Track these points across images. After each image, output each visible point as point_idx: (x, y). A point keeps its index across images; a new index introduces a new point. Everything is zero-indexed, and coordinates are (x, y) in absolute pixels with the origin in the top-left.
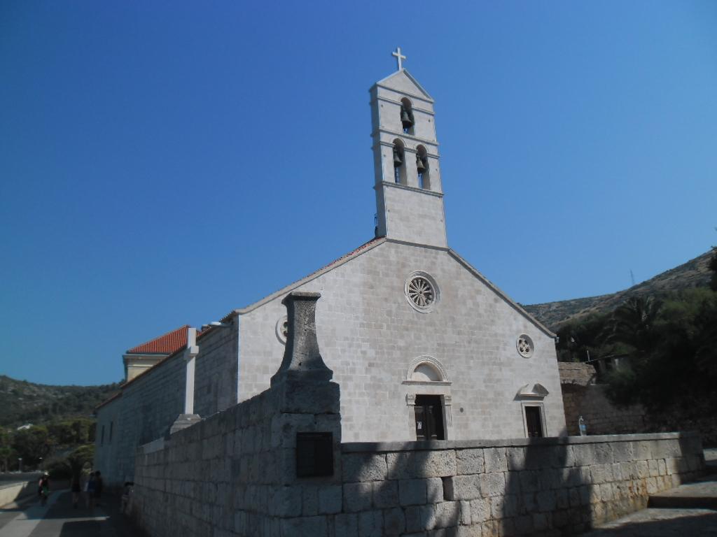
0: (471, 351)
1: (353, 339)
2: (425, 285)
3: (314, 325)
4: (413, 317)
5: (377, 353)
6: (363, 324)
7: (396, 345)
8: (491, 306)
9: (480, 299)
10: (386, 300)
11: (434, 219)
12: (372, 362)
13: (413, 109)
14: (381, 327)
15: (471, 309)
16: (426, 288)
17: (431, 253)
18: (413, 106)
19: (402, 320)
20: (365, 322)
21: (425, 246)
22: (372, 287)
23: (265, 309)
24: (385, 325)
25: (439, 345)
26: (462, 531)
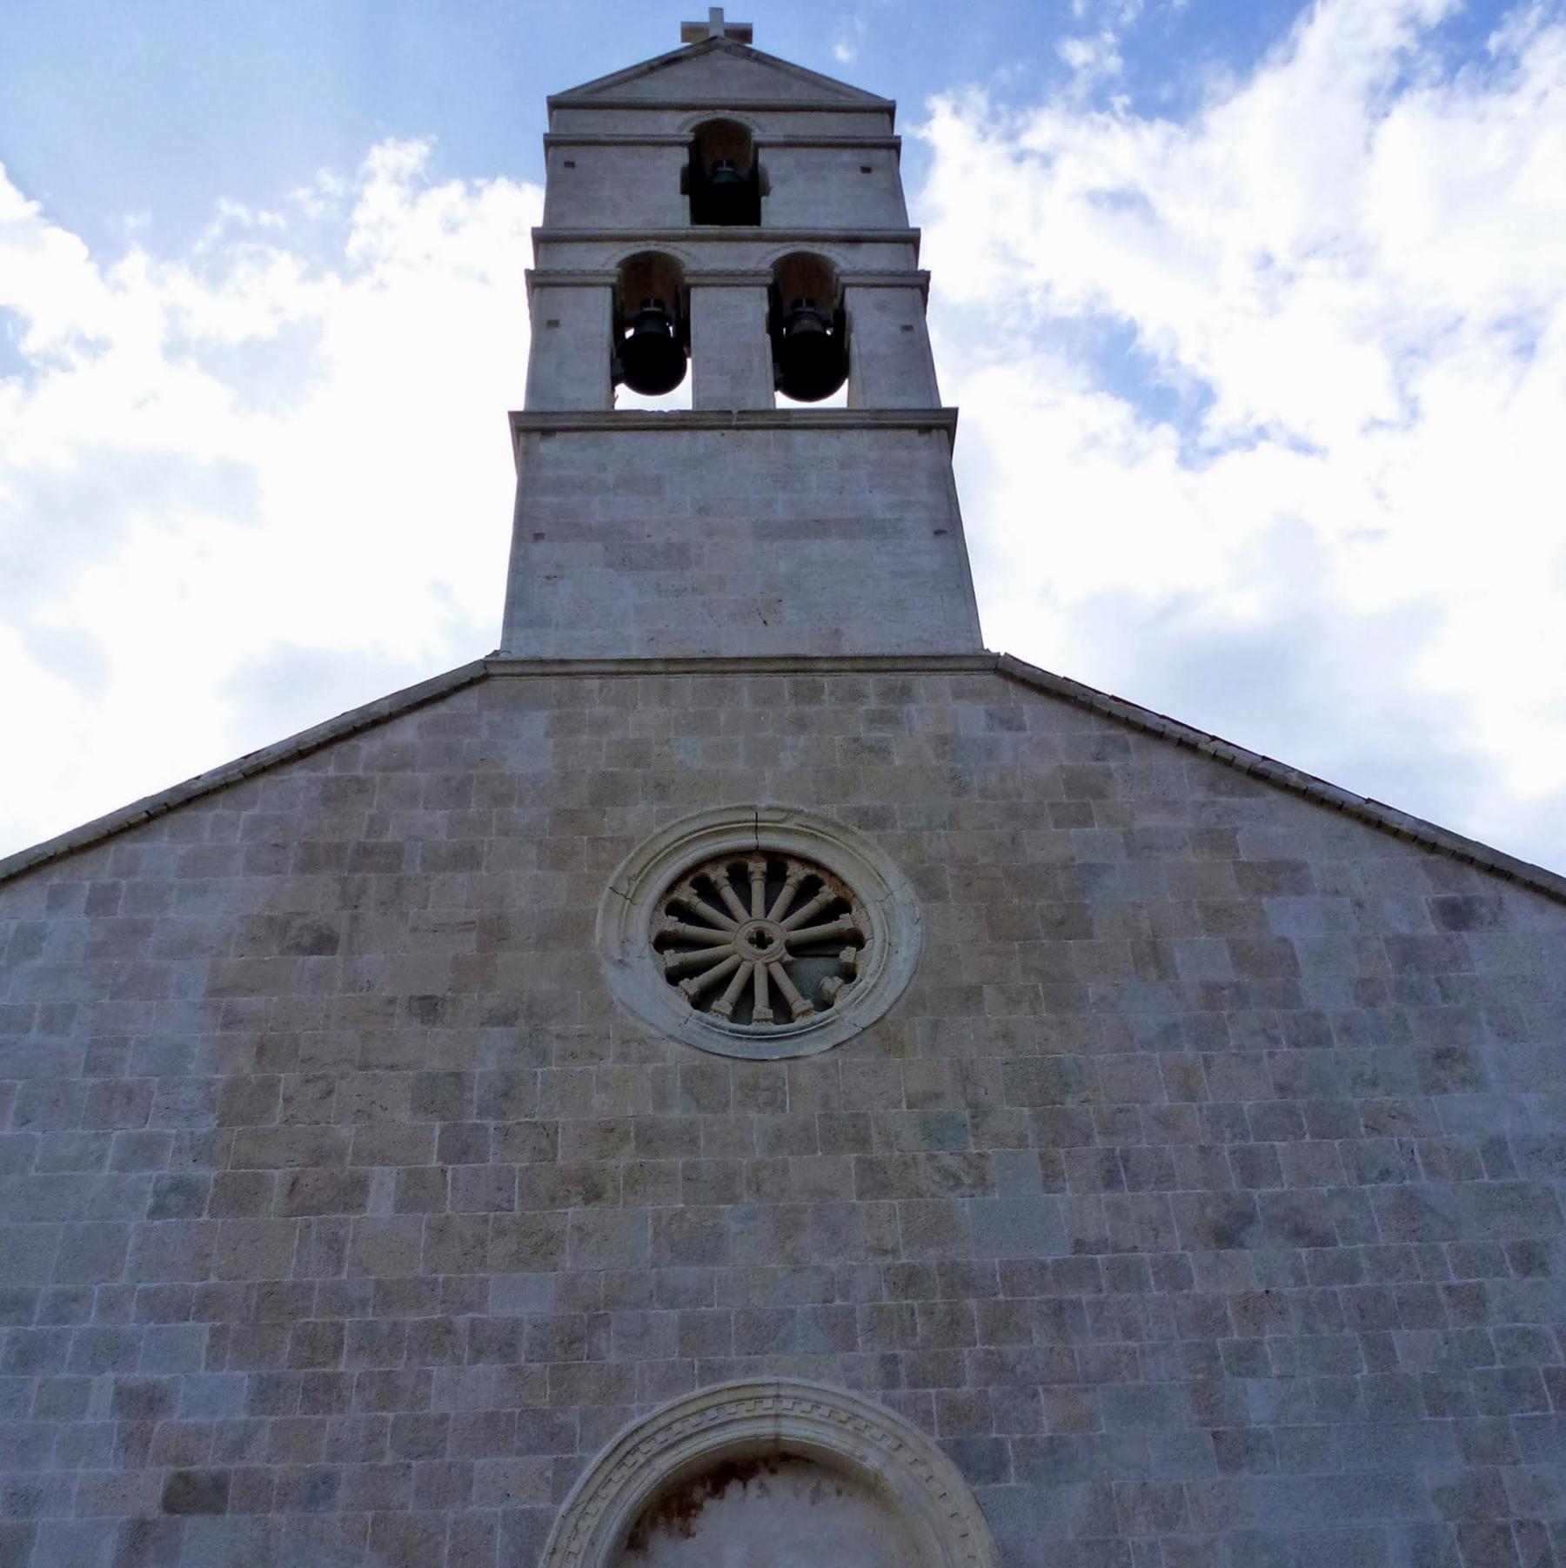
0: (1246, 1306)
1: (63, 1309)
2: (740, 878)
3: (1099, 100)
4: (662, 1101)
5: (266, 1393)
6: (184, 1188)
7: (461, 1321)
8: (1409, 952)
9: (1292, 921)
10: (429, 1008)
11: (874, 528)
12: (207, 1465)
13: (758, 145)
14: (353, 1192)
15: (1211, 991)
16: (729, 895)
17: (857, 696)
18: (757, 136)
19: (550, 1131)
20: (207, 1174)
21: (798, 665)
22: (324, 942)
23: (667, 687)
24: (384, 1182)
25: (910, 1281)
26: (13, 390)
